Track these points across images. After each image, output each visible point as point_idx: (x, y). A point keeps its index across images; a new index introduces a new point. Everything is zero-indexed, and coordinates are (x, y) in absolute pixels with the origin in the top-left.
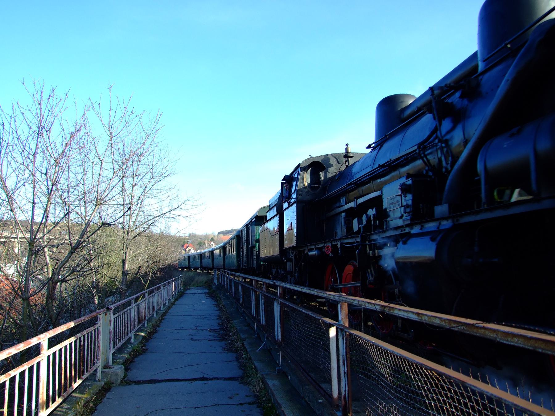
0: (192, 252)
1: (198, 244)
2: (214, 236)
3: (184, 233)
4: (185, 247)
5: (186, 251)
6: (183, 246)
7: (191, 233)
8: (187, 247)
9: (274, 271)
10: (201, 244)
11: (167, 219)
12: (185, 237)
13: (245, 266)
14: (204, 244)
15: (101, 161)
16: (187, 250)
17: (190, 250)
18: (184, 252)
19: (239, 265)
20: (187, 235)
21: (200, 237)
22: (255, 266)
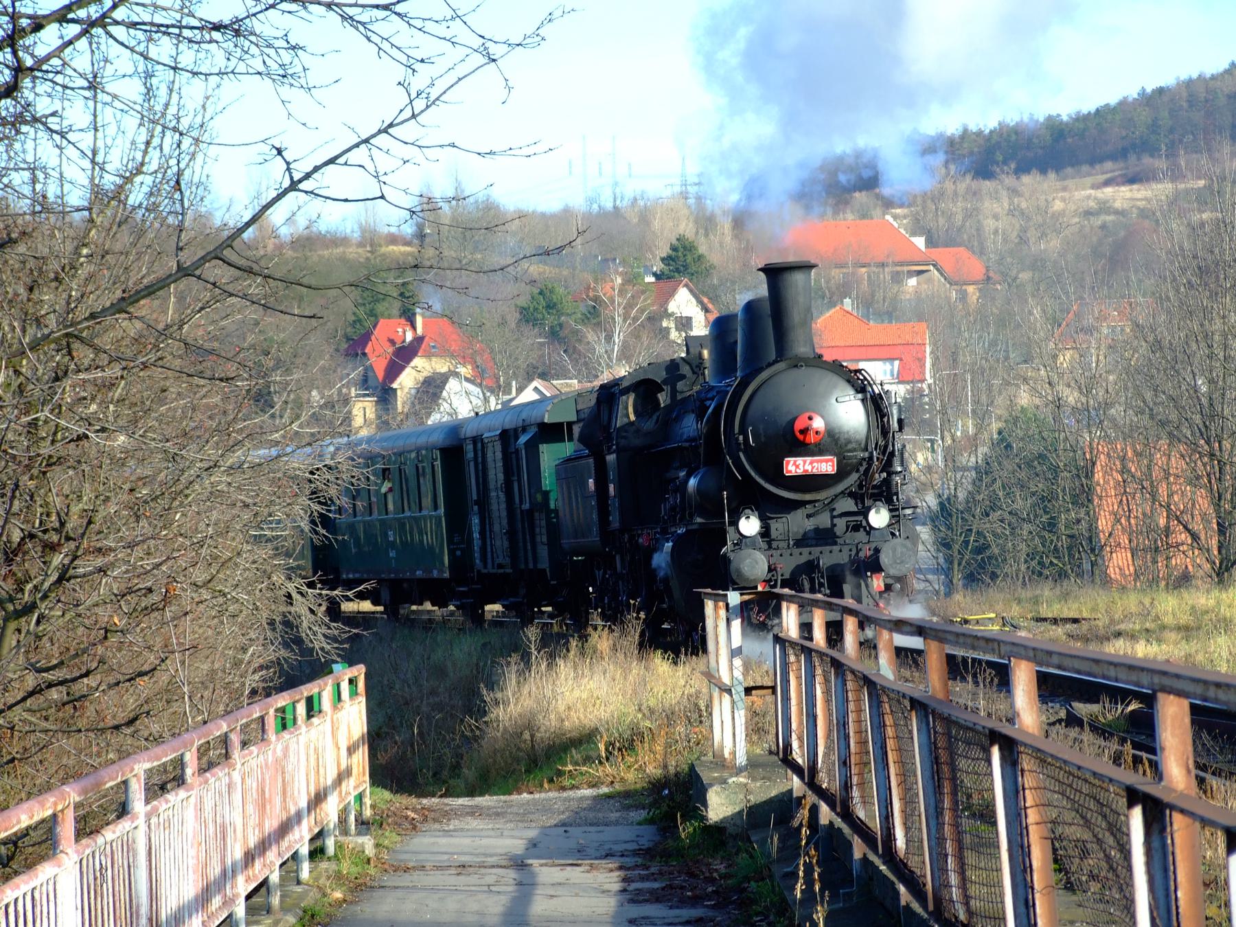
0: (463, 402)
1: (528, 316)
2: (706, 222)
3: (354, 208)
4: (378, 355)
5: (385, 395)
6: (356, 346)
7: (442, 189)
8: (404, 355)
9: (599, 574)
10: (551, 319)
11: (163, 49)
12: (371, 239)
13: (500, 566)
14: (595, 314)
15: (52, 131)
16: (407, 382)
17: (432, 388)
18: (363, 411)
19: (460, 565)
20: (392, 219)
21: (556, 239)
22: (544, 564)
